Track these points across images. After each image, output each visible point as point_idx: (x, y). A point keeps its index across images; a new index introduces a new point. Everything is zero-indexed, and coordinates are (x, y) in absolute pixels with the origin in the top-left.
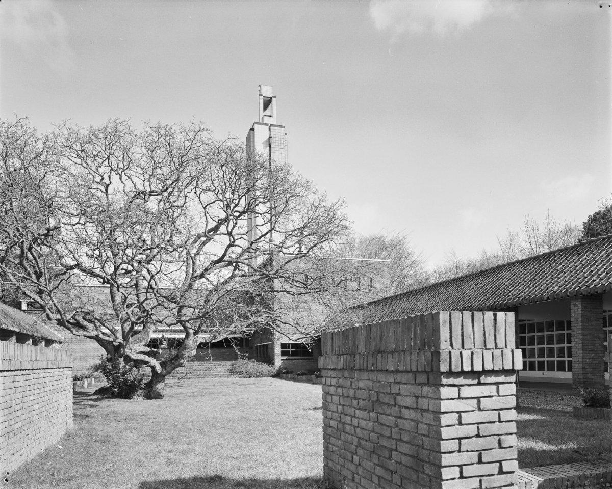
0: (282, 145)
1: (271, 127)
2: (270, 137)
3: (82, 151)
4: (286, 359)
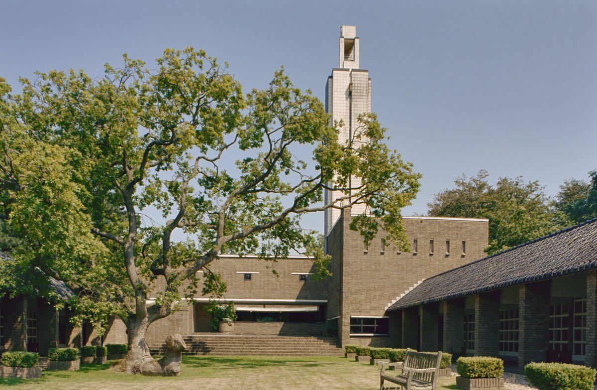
0: (365, 91)
1: (353, 73)
2: (351, 84)
3: (126, 75)
4: (373, 336)
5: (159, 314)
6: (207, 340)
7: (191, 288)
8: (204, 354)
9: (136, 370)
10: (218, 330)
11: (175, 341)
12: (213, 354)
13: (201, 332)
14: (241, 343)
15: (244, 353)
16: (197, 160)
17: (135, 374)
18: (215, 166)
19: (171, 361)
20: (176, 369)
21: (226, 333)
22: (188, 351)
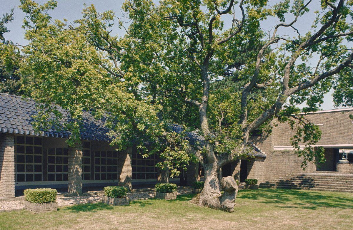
5: (227, 159)
6: (315, 178)
7: (297, 137)
8: (309, 189)
9: (205, 203)
10: (334, 169)
11: (226, 182)
12: (315, 190)
13: (323, 171)
14: (344, 182)
15: (342, 190)
16: (276, 28)
17: (205, 206)
18: (295, 29)
19: (226, 198)
20: (229, 205)
21: (341, 172)
22: (296, 186)
